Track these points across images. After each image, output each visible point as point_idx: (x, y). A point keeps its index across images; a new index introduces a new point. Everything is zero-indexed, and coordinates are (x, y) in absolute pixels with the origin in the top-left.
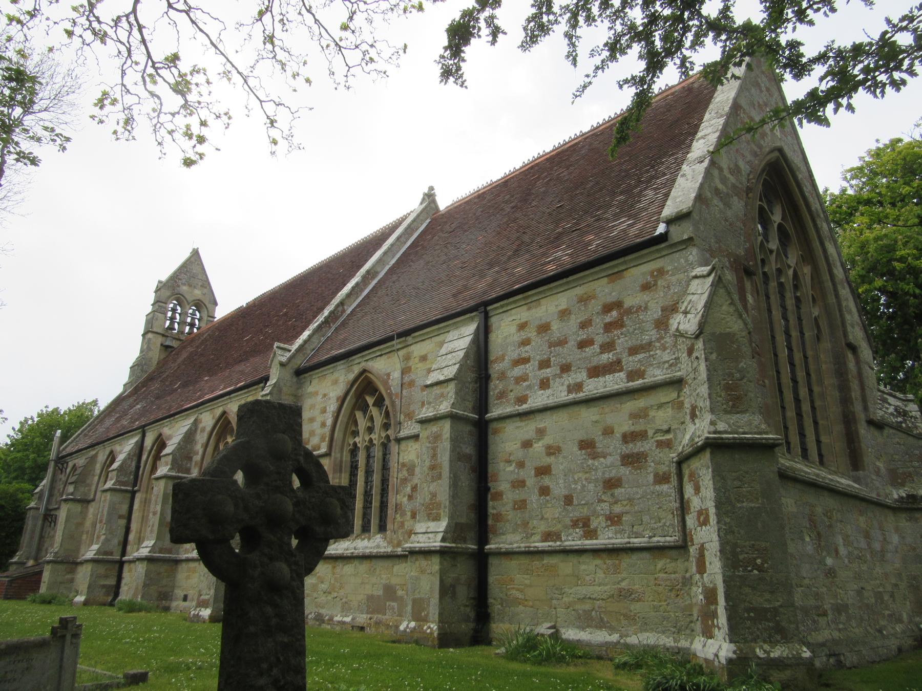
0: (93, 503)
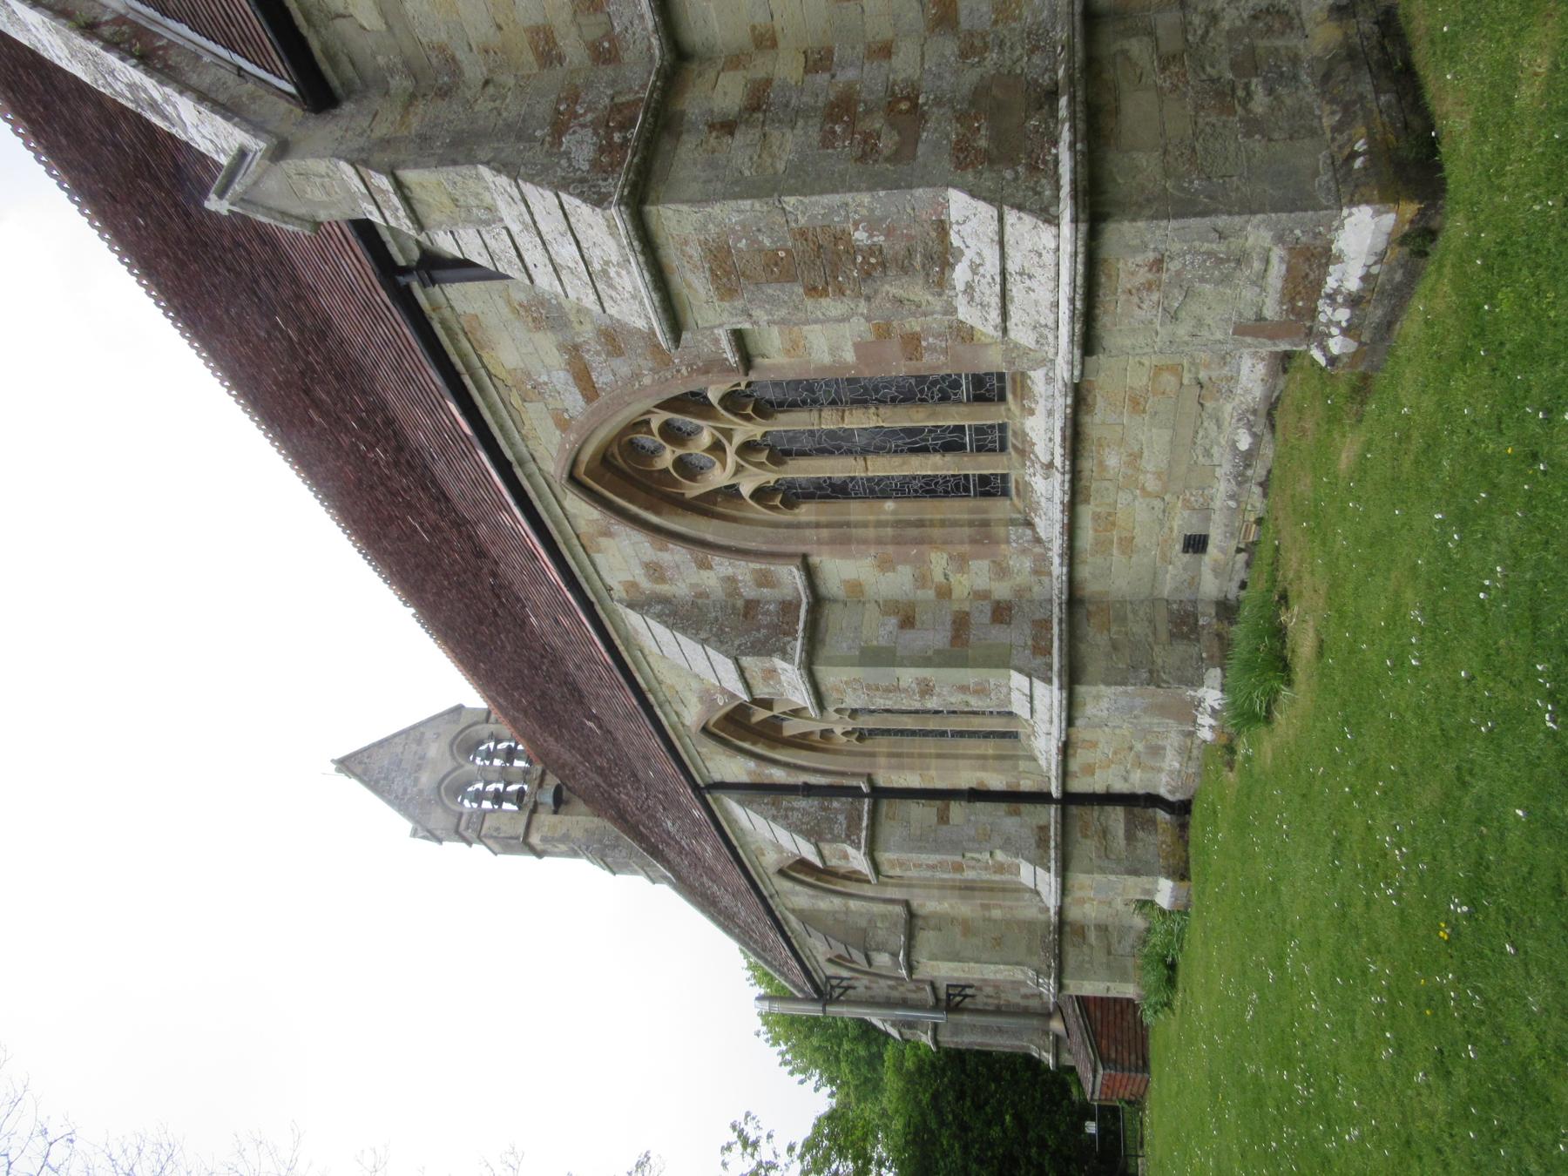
0: (915, 904)
